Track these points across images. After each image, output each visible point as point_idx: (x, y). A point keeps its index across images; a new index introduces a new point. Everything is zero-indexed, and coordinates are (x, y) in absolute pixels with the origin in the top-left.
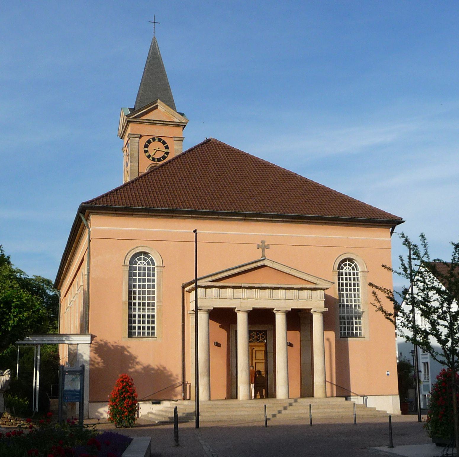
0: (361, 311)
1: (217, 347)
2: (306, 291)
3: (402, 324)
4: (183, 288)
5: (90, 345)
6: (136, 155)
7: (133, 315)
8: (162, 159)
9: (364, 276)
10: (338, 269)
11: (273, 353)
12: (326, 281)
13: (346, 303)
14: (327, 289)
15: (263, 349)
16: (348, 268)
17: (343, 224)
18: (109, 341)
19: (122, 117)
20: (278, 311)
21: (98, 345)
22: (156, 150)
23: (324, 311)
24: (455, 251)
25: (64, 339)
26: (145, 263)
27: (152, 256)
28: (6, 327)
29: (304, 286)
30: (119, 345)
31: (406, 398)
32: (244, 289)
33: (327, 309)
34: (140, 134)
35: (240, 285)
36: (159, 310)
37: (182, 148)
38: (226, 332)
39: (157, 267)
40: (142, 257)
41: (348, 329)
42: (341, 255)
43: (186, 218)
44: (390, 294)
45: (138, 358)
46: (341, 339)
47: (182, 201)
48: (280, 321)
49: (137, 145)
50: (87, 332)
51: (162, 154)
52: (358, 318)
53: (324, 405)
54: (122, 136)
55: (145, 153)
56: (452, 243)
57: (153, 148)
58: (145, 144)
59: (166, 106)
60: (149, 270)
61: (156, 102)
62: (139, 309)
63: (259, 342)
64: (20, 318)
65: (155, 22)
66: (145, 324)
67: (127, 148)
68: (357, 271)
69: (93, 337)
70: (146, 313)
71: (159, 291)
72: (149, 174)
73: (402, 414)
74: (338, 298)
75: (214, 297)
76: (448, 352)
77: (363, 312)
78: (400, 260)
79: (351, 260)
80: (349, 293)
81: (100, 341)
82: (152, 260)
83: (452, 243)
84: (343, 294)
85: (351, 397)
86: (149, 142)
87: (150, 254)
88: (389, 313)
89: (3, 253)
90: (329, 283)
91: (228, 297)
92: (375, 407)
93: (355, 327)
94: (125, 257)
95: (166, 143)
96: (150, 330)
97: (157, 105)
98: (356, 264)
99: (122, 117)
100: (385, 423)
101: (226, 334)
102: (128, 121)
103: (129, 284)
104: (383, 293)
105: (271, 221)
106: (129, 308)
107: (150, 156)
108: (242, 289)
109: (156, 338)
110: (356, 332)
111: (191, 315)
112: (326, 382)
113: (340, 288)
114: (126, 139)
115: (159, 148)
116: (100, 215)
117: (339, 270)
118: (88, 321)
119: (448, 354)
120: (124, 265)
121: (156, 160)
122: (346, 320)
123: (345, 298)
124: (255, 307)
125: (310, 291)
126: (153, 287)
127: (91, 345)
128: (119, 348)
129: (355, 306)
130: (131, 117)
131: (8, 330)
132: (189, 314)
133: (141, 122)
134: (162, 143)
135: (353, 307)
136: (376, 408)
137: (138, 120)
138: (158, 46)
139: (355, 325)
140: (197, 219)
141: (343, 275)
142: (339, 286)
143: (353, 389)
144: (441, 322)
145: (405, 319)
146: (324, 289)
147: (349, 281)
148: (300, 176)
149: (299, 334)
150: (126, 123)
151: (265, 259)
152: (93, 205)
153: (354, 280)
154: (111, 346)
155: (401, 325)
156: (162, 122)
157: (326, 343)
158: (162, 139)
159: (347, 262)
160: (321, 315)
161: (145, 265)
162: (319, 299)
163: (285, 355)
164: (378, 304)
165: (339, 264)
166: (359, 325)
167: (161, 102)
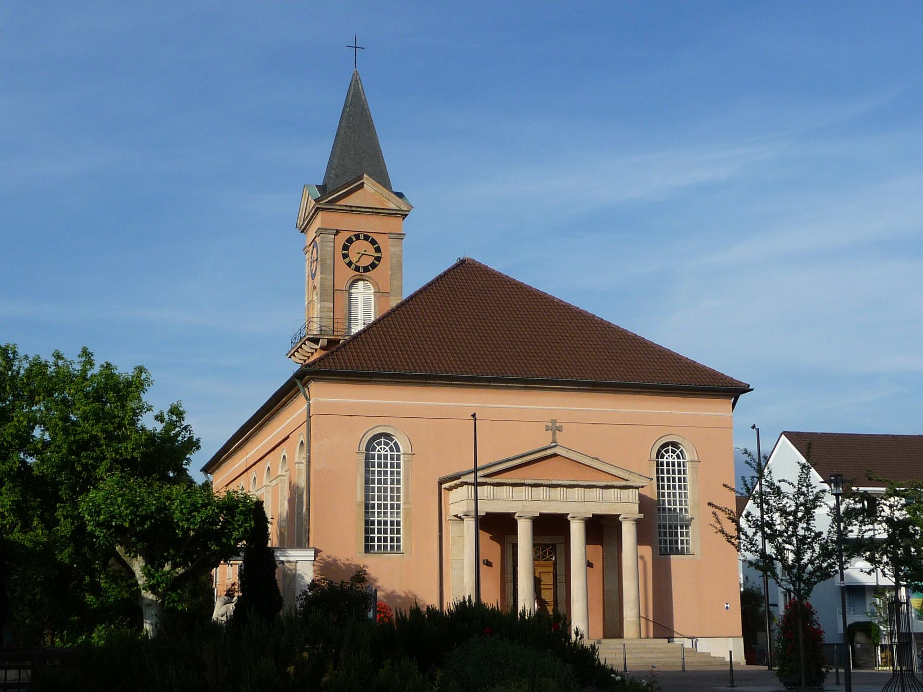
0: (690, 517)
1: (488, 567)
2: (613, 490)
3: (745, 547)
4: (441, 483)
5: (313, 563)
6: (330, 262)
7: (371, 520)
8: (370, 267)
9: (694, 468)
10: (657, 457)
11: (564, 576)
12: (642, 476)
13: (668, 505)
14: (642, 487)
15: (551, 569)
16: (670, 456)
17: (665, 393)
18: (339, 557)
19: (305, 198)
20: (574, 517)
21: (324, 564)
22: (360, 254)
23: (638, 518)
24: (801, 471)
25: (278, 555)
26: (387, 448)
27: (396, 440)
28: (228, 540)
29: (610, 483)
30: (353, 563)
31: (755, 644)
32: (527, 487)
33: (643, 515)
34: (335, 228)
35: (522, 481)
36: (407, 515)
37: (401, 251)
38: (499, 546)
39: (404, 454)
40: (383, 440)
41: (671, 543)
42: (661, 438)
43: (444, 386)
44: (732, 514)
45: (378, 581)
46: (662, 556)
47: (437, 361)
48: (577, 531)
49: (331, 246)
50: (307, 545)
51: (371, 260)
52: (684, 528)
53: (639, 648)
54: (305, 229)
55: (344, 259)
56: (799, 463)
57: (357, 251)
58: (344, 244)
59: (377, 184)
60: (392, 459)
61: (361, 178)
62: (391, 513)
63: (545, 560)
64: (246, 529)
65: (357, 46)
66: (387, 534)
67: (313, 247)
68: (684, 460)
69: (317, 552)
70: (389, 519)
71: (406, 489)
72: (385, 319)
73: (747, 664)
74: (657, 499)
75: (486, 498)
76: (794, 579)
77: (692, 518)
78: (742, 481)
79: (675, 445)
80: (672, 491)
81: (327, 558)
82: (396, 444)
83: (799, 463)
84: (663, 494)
85: (675, 639)
86: (350, 241)
87: (393, 436)
88: (730, 535)
89: (191, 435)
90: (646, 479)
91: (505, 498)
92: (709, 652)
93: (681, 539)
94: (359, 441)
95: (377, 243)
96: (394, 543)
97: (363, 183)
98: (682, 449)
99: (305, 198)
100: (727, 671)
101: (500, 548)
102: (317, 208)
103: (365, 478)
104: (724, 513)
105: (562, 390)
106: (365, 511)
107: (352, 263)
108: (524, 487)
109: (403, 553)
110: (681, 547)
111: (452, 521)
112: (641, 618)
113: (659, 484)
114: (312, 233)
115: (365, 251)
116: (326, 382)
117: (658, 458)
118: (309, 529)
119: (794, 581)
120: (359, 452)
121: (361, 270)
122: (668, 530)
123: (666, 499)
124: (543, 512)
125: (619, 490)
126: (398, 482)
127: (315, 562)
128: (353, 567)
129: (681, 509)
130: (321, 202)
131: (230, 544)
132: (448, 520)
133: (338, 210)
134: (370, 242)
135: (678, 511)
136: (710, 653)
137: (333, 207)
138: (362, 85)
139: (681, 537)
140: (459, 387)
141: (663, 466)
142: (658, 481)
143: (677, 628)
144: (787, 546)
145: (748, 542)
146: (637, 488)
147: (672, 474)
148: (600, 320)
149: (602, 549)
150: (314, 210)
151: (557, 445)
152: (317, 368)
153: (679, 473)
154: (342, 565)
155: (744, 549)
156: (371, 210)
157: (640, 562)
158: (370, 237)
159: (670, 448)
160: (633, 524)
161: (387, 451)
162: (631, 500)
163: (584, 581)
164: (719, 526)
165: (659, 449)
166: (686, 537)
167: (369, 178)
